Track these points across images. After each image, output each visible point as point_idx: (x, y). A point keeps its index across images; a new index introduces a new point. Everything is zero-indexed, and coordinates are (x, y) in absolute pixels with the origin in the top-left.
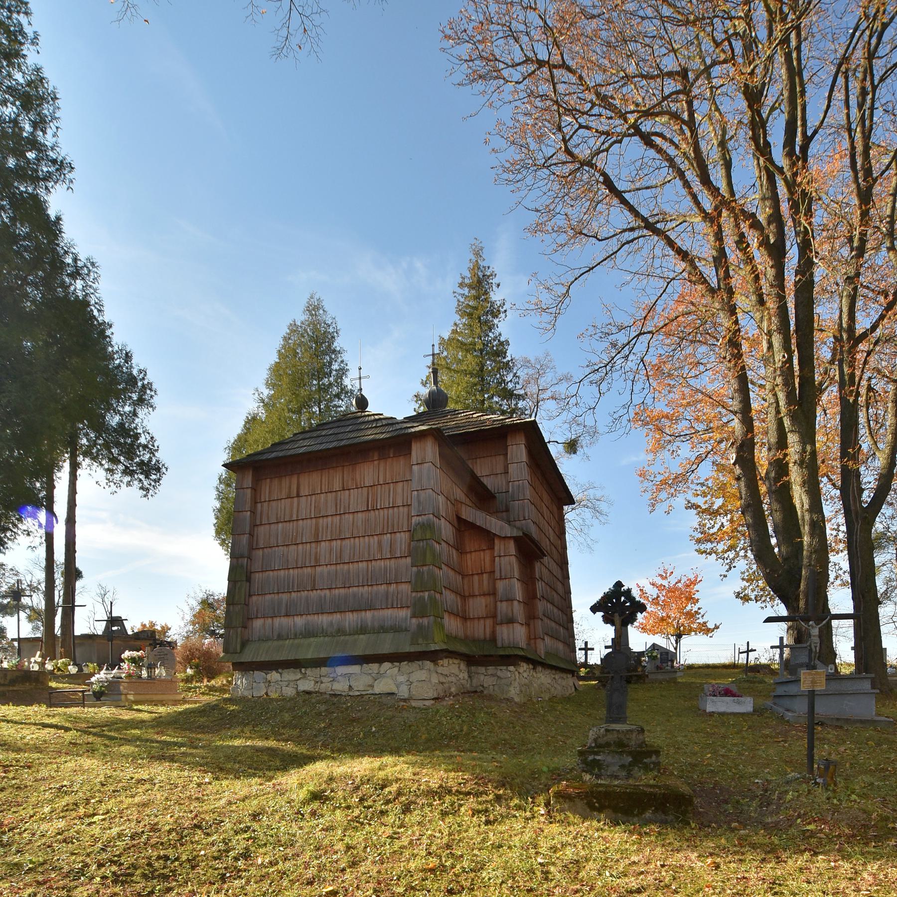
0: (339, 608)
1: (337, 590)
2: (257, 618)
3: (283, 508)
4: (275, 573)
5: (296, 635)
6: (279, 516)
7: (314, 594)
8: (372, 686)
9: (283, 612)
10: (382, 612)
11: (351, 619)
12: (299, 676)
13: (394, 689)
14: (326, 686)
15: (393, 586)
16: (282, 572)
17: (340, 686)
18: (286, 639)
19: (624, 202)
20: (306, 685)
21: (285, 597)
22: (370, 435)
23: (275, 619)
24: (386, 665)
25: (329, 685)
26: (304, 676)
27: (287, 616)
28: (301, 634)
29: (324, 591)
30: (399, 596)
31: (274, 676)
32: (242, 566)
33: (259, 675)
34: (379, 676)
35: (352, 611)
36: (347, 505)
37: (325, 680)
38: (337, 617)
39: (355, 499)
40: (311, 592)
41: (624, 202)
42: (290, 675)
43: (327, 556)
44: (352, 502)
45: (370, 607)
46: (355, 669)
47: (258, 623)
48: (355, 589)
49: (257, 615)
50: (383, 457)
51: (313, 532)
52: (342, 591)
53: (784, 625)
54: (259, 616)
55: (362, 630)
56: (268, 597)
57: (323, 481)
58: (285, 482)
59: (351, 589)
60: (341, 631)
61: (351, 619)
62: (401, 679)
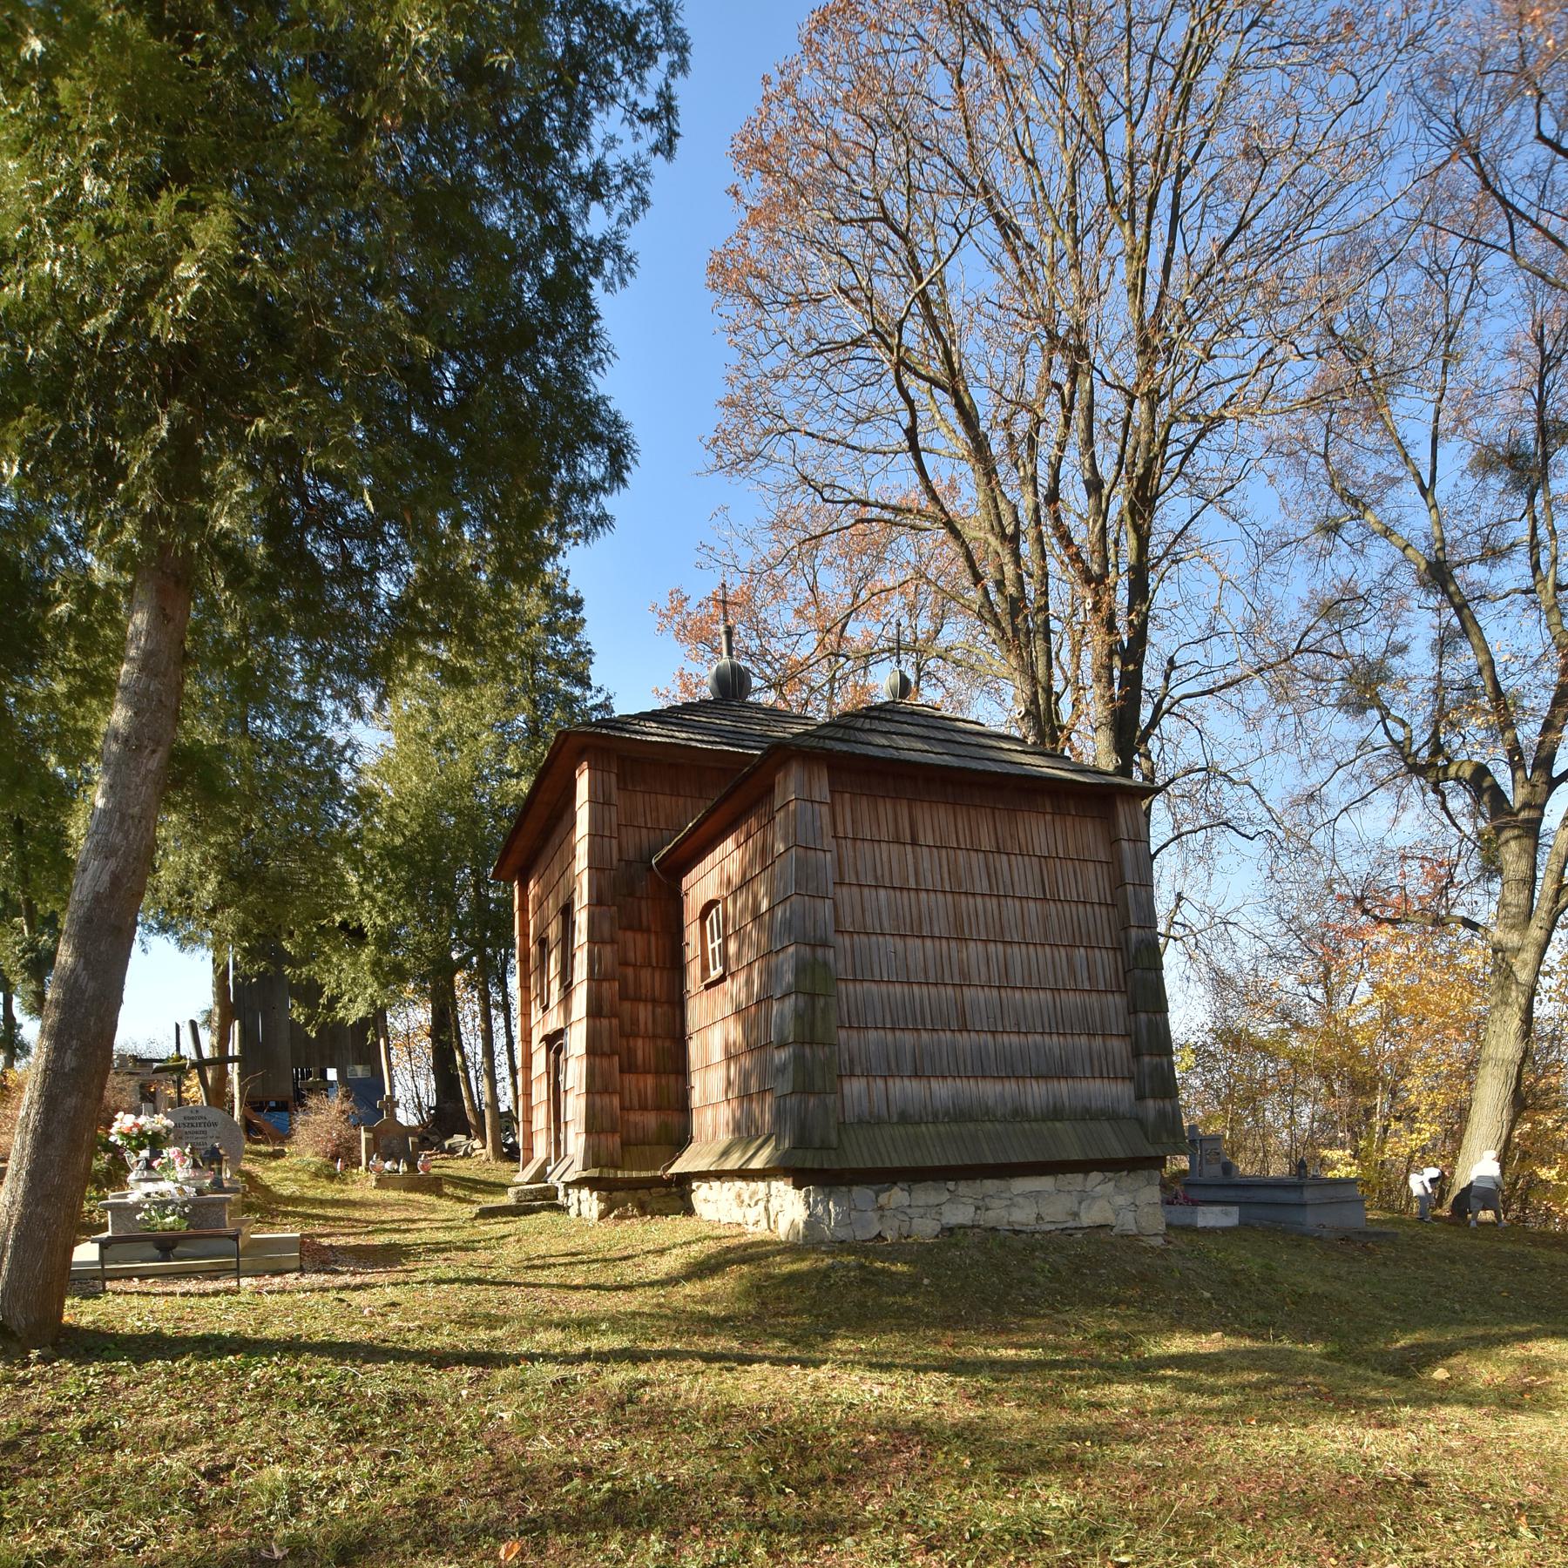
0: (1011, 1068)
1: (1005, 1036)
2: (852, 1075)
3: (885, 858)
4: (884, 987)
5: (936, 1115)
6: (879, 873)
7: (963, 1039)
8: (1076, 1215)
9: (908, 1071)
10: (1084, 1083)
11: (1037, 1092)
12: (946, 1196)
13: (1111, 1220)
14: (997, 1215)
15: (1099, 1040)
16: (898, 987)
17: (1023, 1216)
18: (919, 1123)
19: (918, 459)
20: (960, 1215)
21: (908, 1038)
22: (913, 749)
23: (890, 1082)
24: (1095, 1177)
25: (1003, 1213)
26: (954, 1198)
27: (916, 1076)
28: (947, 1113)
29: (983, 1036)
30: (1110, 1059)
31: (897, 1196)
32: (825, 964)
33: (862, 1194)
34: (1083, 1196)
35: (1037, 1078)
36: (1008, 881)
37: (996, 1203)
38: (1011, 1087)
39: (1020, 873)
40: (958, 1035)
41: (918, 459)
42: (926, 1195)
43: (983, 969)
44: (1016, 878)
45: (1065, 1073)
46: (1044, 1183)
47: (854, 1087)
48: (1038, 1038)
49: (852, 1069)
50: (1059, 812)
51: (951, 919)
52: (1014, 1039)
53: (194, 1057)
54: (858, 1071)
55: (1055, 1113)
56: (872, 1035)
57: (960, 826)
58: (886, 809)
59: (1030, 1038)
60: (1019, 1114)
61: (1037, 1092)
62: (1120, 1200)
